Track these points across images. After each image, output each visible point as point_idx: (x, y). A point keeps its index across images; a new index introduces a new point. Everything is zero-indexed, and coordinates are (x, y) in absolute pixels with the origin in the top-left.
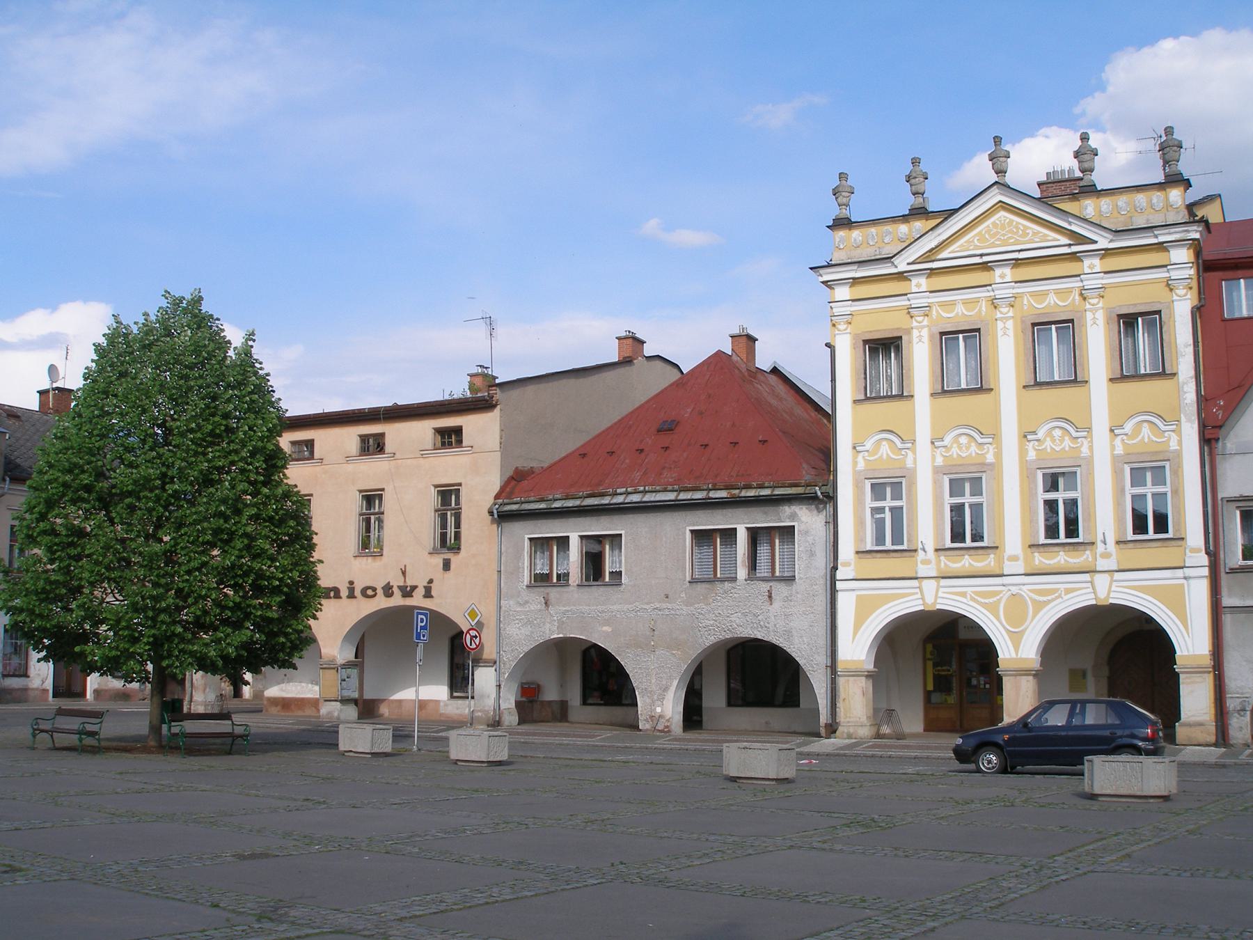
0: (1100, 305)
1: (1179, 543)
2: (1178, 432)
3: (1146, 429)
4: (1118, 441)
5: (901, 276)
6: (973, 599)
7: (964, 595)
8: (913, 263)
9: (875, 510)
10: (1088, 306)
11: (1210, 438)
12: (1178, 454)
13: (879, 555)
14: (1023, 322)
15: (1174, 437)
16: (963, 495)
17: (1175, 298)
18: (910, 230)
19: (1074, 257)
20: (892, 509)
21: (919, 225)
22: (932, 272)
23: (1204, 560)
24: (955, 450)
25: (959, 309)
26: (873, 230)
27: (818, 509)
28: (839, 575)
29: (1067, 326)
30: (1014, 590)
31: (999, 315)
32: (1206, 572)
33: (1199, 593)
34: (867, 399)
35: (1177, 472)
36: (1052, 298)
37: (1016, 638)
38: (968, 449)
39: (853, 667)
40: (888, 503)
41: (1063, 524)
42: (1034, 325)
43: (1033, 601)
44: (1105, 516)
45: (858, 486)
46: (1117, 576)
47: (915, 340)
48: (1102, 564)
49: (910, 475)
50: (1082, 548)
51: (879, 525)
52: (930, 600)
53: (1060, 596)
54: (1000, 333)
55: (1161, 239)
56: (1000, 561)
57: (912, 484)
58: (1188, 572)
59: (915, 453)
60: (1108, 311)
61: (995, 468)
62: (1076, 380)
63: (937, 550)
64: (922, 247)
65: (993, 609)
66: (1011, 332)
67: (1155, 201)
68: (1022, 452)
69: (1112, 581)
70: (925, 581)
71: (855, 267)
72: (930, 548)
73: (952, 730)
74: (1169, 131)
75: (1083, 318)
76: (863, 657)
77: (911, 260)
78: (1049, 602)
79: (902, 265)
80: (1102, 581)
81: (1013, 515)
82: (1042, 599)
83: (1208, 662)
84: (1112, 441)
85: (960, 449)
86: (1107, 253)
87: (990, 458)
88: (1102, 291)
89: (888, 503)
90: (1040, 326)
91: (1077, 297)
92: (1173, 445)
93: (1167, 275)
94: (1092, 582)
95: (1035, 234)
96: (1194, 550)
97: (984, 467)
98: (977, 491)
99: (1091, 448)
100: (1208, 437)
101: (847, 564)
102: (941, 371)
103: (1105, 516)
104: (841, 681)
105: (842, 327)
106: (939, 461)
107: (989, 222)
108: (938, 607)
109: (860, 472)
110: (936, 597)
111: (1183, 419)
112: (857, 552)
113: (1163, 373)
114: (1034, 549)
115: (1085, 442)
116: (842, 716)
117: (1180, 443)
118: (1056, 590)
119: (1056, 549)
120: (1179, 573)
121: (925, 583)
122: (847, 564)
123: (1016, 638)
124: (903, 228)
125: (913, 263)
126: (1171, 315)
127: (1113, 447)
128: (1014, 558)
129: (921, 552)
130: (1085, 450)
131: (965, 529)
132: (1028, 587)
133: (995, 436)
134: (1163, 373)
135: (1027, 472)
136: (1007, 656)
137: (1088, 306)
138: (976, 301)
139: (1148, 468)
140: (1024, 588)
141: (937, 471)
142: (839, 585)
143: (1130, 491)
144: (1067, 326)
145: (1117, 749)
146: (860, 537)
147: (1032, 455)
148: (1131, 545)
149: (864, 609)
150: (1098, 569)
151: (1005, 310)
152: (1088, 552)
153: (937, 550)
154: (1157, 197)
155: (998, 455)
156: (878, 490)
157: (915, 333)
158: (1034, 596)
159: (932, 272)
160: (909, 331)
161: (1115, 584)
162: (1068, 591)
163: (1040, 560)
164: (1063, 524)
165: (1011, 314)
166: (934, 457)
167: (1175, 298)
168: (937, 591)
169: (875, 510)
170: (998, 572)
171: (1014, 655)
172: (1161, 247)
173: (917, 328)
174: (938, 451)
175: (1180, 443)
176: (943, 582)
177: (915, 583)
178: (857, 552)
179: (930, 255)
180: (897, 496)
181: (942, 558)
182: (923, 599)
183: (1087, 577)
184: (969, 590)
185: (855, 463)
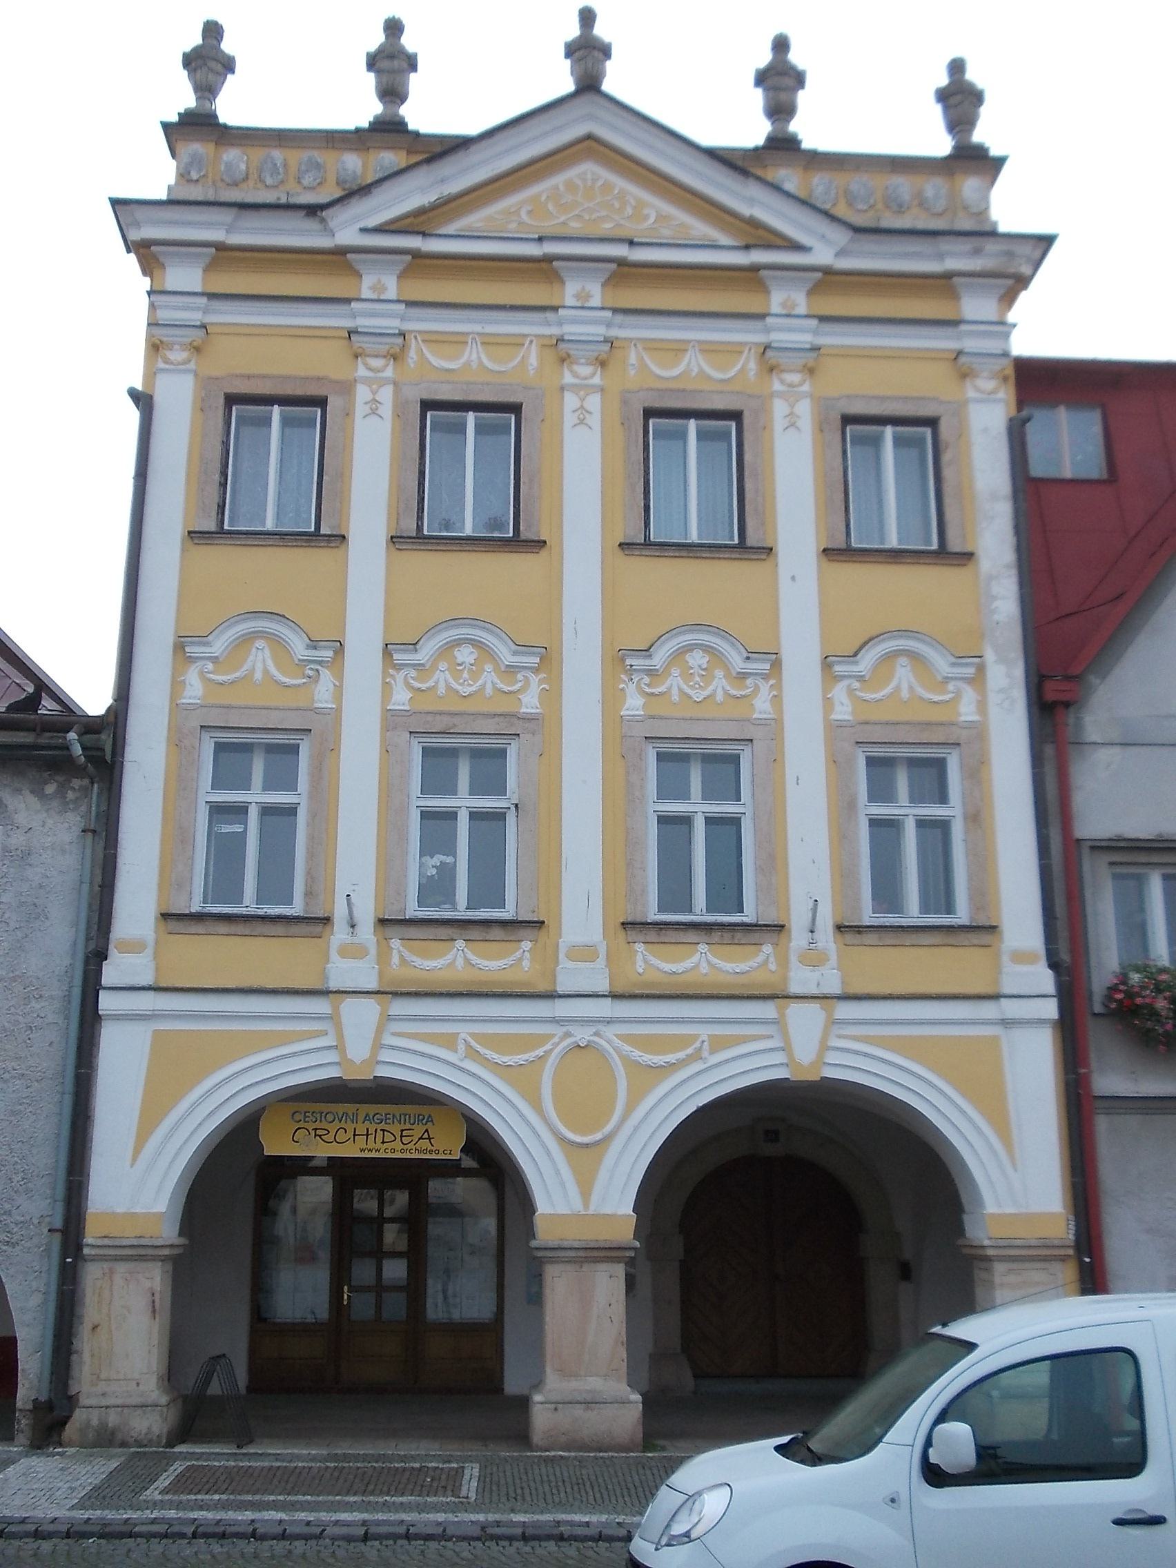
0: (806, 388)
1: (985, 938)
2: (978, 679)
3: (903, 674)
4: (839, 692)
5: (339, 259)
6: (472, 1054)
7: (449, 1042)
8: (380, 230)
9: (219, 811)
10: (777, 386)
11: (1053, 707)
12: (979, 732)
13: (223, 928)
14: (625, 402)
15: (969, 696)
16: (452, 791)
17: (971, 394)
18: (365, 165)
19: (751, 277)
20: (268, 811)
21: (391, 159)
22: (420, 263)
23: (1046, 980)
24: (442, 678)
25: (472, 352)
26: (278, 155)
27: (61, 792)
28: (111, 973)
29: (727, 422)
30: (583, 1035)
31: (568, 378)
32: (1051, 1009)
33: (1033, 1065)
34: (221, 532)
35: (977, 772)
36: (694, 357)
37: (585, 1157)
38: (475, 675)
39: (129, 1234)
40: (255, 797)
41: (700, 884)
42: (649, 413)
43: (633, 1066)
44: (808, 851)
45: (178, 741)
46: (846, 1010)
47: (360, 409)
48: (802, 979)
49: (324, 731)
50: (756, 937)
51: (226, 855)
52: (358, 1051)
53: (696, 1056)
54: (569, 419)
55: (951, 264)
56: (549, 960)
57: (329, 750)
58: (1011, 1009)
59: (339, 676)
60: (822, 405)
61: (543, 728)
62: (747, 546)
63: (382, 922)
64: (941, 257)
65: (524, 1080)
66: (595, 420)
67: (929, 192)
68: (611, 698)
69: (832, 1022)
70: (349, 1001)
71: (227, 216)
72: (366, 914)
73: (250, 1380)
74: (957, 67)
75: (764, 408)
76: (161, 1206)
77: (372, 222)
78: (672, 1067)
79: (346, 229)
80: (805, 1023)
81: (583, 855)
82: (647, 1058)
83: (1063, 1230)
84: (826, 689)
85: (457, 674)
86: (829, 280)
87: (530, 703)
88: (813, 361)
89: (255, 797)
90: (661, 415)
91: (752, 365)
92: (967, 711)
93: (761, 338)
94: (334, 1018)
95: (661, 218)
96: (1020, 957)
97: (516, 725)
98: (491, 782)
99: (777, 700)
100: (1050, 696)
101: (135, 947)
102: (418, 484)
103: (808, 851)
104: (92, 1275)
105: (177, 355)
106: (401, 698)
107: (558, 180)
108: (382, 1072)
109: (190, 708)
110: (378, 1046)
111: (990, 656)
112: (166, 916)
113: (949, 555)
114: (633, 935)
115: (765, 688)
116: (85, 1383)
117: (982, 706)
118: (685, 1041)
119: (691, 936)
120: (988, 1010)
121: (349, 1006)
122: (135, 947)
123: (585, 1157)
124: (352, 162)
125: (380, 230)
126: (962, 430)
127: (828, 703)
128: (584, 953)
129: (339, 934)
130: (762, 706)
131: (470, 899)
132: (618, 1032)
133: (548, 659)
134: (949, 555)
135: (620, 741)
136: (562, 1209)
137: (777, 386)
138: (516, 342)
139: (907, 763)
140: (610, 1031)
141: (391, 720)
142: (106, 1002)
143: (300, 797)
144: (727, 422)
145: (555, 976)
146: (170, 877)
147: (634, 704)
148: (871, 938)
149: (169, 1076)
150: (1007, 990)
151: (585, 370)
152: (767, 949)
153: (382, 922)
154: (933, 187)
155: (553, 696)
156: (232, 755)
157: (362, 393)
158: (637, 1054)
159: (420, 263)
160: (347, 388)
161: (836, 1030)
162: (718, 1044)
163: (650, 962)
164: (700, 884)
165: (597, 380)
166: (387, 688)
167: (971, 394)
168: (380, 1031)
169: (219, 811)
170: (542, 987)
171: (577, 1205)
172: (944, 284)
173: (367, 381)
174: (400, 677)
175: (982, 706)
176: (400, 1007)
177: (320, 1006)
178: (166, 916)
179: (418, 222)
180: (283, 779)
181: (396, 943)
182: (339, 1047)
183: (767, 1010)
184: (463, 1030)
185: (177, 685)
